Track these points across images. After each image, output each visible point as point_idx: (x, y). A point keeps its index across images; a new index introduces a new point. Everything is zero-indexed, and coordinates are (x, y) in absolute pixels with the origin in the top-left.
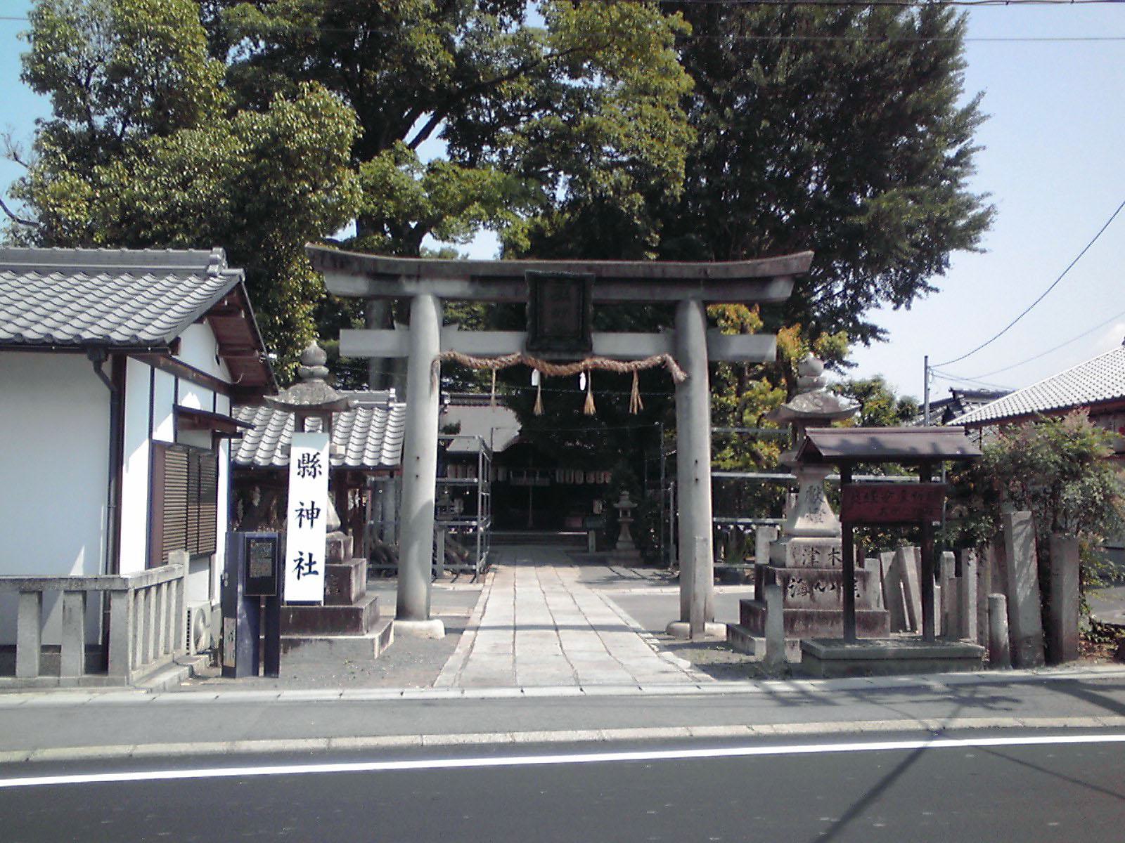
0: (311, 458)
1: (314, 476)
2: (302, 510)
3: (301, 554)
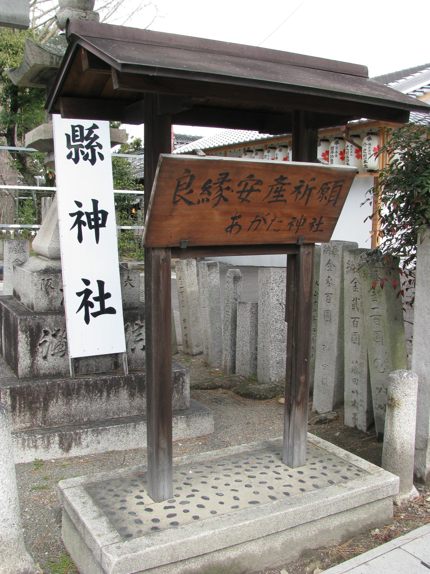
0: (86, 133)
1: (93, 161)
2: (88, 292)
3: (87, 282)
